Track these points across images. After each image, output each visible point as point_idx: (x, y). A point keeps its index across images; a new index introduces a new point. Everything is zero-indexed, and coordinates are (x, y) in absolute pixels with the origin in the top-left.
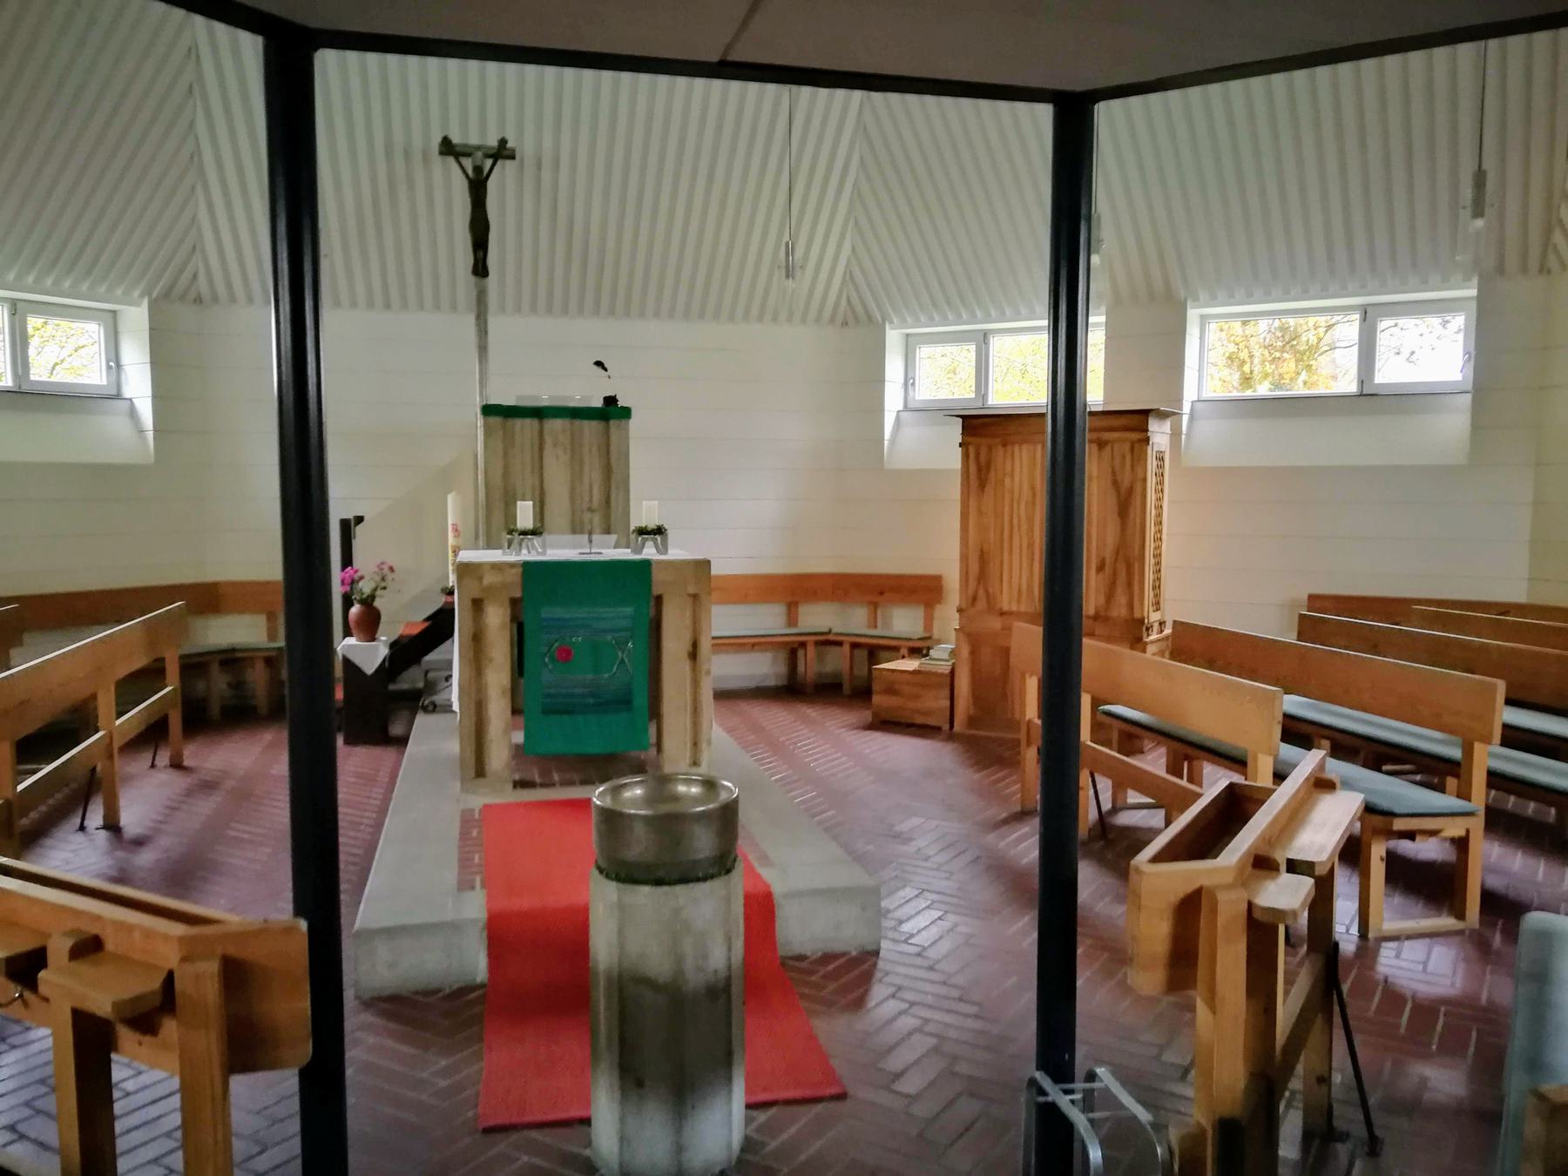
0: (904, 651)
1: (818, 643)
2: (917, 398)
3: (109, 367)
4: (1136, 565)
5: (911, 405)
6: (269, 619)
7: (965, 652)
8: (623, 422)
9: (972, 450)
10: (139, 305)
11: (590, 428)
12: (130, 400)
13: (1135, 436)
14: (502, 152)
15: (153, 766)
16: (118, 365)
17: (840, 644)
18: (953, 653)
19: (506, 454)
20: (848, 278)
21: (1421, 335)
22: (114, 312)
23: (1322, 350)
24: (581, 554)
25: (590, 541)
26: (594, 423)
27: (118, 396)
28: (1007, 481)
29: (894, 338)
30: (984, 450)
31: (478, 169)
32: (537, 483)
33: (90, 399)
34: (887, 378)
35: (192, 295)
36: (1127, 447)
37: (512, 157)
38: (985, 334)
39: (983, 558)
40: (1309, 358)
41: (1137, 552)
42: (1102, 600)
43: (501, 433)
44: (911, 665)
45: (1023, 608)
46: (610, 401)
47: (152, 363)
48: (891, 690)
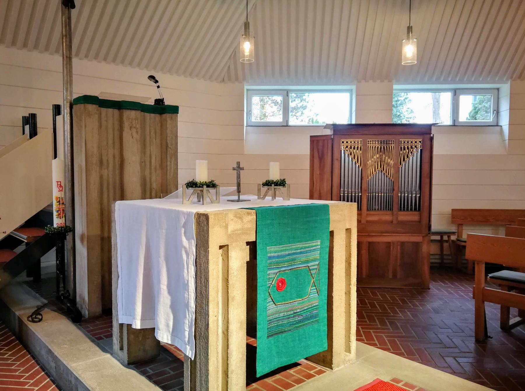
8: (174, 115)
26: (153, 115)
43: (97, 116)
46: (159, 102)
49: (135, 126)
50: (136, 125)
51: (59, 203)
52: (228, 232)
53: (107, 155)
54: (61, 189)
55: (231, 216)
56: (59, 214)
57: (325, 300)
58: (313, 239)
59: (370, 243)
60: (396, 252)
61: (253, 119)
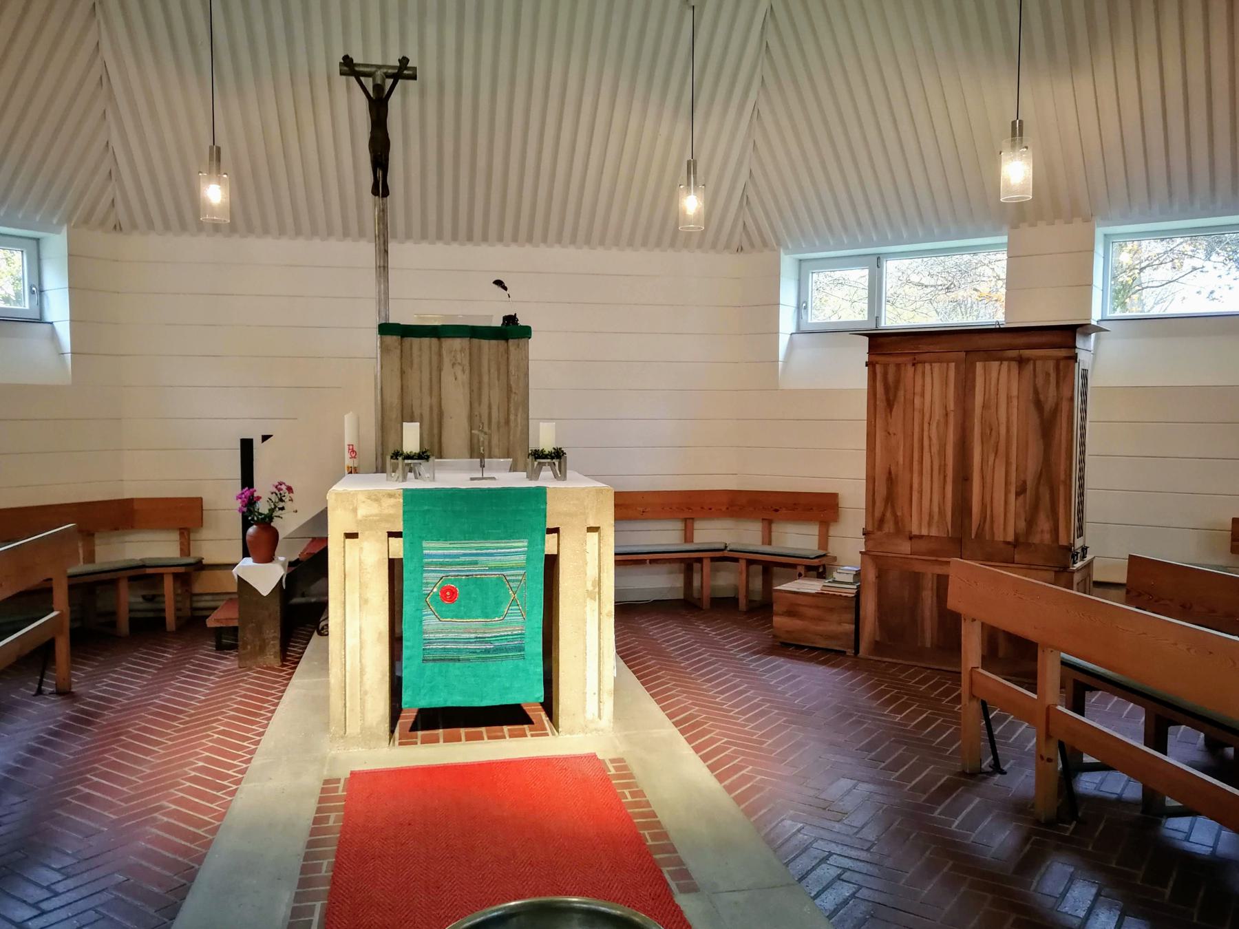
0: (801, 569)
1: (713, 559)
2: (809, 321)
3: (32, 292)
4: (1062, 488)
5: (803, 328)
6: (182, 534)
7: (871, 575)
9: (879, 369)
10: (59, 233)
11: (488, 347)
12: (51, 323)
13: (1063, 353)
14: (403, 71)
15: (40, 692)
16: (41, 291)
17: (736, 560)
18: (857, 575)
19: (402, 372)
21: (1220, 276)
22: (38, 240)
23: (1133, 290)
24: (472, 479)
25: (483, 466)
26: (493, 342)
27: (40, 321)
28: (917, 401)
29: (787, 263)
30: (892, 371)
31: (378, 88)
33: (25, 323)
34: (781, 302)
35: (111, 222)
36: (1051, 365)
37: (414, 77)
38: (878, 258)
39: (891, 480)
40: (1123, 296)
41: (1062, 477)
42: (1022, 524)
43: (398, 351)
44: (812, 586)
45: (934, 533)
46: (510, 320)
47: (70, 288)
48: (791, 613)
49: (459, 361)
50: (462, 360)
52: (356, 515)
53: (421, 406)
55: (361, 497)
57: (538, 628)
58: (511, 536)
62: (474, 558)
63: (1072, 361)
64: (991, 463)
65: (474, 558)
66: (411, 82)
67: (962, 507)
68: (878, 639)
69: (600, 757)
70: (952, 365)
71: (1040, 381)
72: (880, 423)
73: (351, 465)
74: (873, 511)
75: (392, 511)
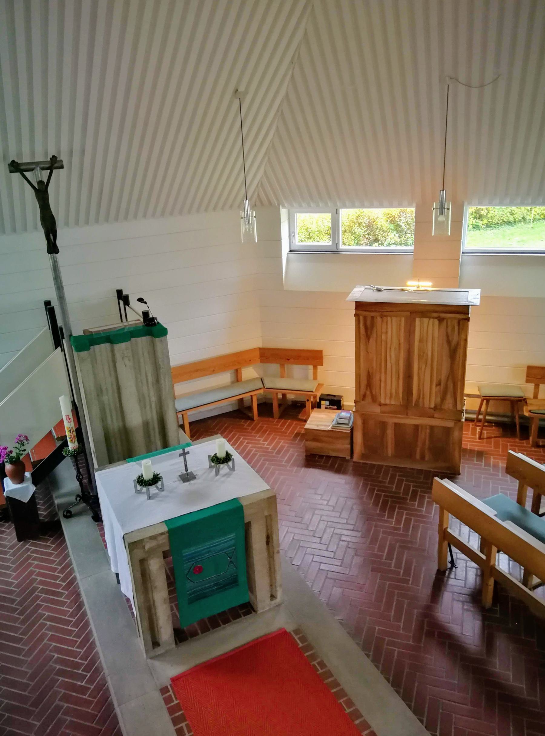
7: (359, 422)
8: (163, 338)
9: (361, 318)
20: (259, 185)
28: (383, 337)
29: (284, 213)
32: (114, 380)
36: (455, 323)
39: (369, 377)
41: (459, 377)
42: (439, 400)
45: (393, 402)
51: (70, 432)
54: (70, 421)
56: (72, 440)
59: (396, 424)
60: (424, 435)
61: (298, 243)
62: (209, 550)
63: (466, 321)
64: (423, 369)
65: (209, 550)
66: (61, 170)
67: (408, 391)
68: (363, 452)
69: (288, 630)
70: (403, 319)
71: (450, 329)
72: (362, 346)
73: (69, 426)
74: (360, 391)
75: (164, 541)
